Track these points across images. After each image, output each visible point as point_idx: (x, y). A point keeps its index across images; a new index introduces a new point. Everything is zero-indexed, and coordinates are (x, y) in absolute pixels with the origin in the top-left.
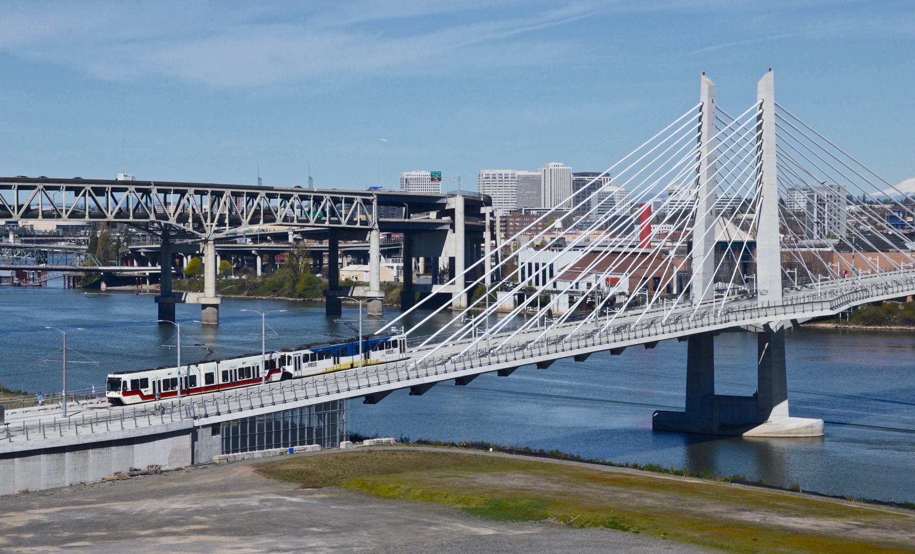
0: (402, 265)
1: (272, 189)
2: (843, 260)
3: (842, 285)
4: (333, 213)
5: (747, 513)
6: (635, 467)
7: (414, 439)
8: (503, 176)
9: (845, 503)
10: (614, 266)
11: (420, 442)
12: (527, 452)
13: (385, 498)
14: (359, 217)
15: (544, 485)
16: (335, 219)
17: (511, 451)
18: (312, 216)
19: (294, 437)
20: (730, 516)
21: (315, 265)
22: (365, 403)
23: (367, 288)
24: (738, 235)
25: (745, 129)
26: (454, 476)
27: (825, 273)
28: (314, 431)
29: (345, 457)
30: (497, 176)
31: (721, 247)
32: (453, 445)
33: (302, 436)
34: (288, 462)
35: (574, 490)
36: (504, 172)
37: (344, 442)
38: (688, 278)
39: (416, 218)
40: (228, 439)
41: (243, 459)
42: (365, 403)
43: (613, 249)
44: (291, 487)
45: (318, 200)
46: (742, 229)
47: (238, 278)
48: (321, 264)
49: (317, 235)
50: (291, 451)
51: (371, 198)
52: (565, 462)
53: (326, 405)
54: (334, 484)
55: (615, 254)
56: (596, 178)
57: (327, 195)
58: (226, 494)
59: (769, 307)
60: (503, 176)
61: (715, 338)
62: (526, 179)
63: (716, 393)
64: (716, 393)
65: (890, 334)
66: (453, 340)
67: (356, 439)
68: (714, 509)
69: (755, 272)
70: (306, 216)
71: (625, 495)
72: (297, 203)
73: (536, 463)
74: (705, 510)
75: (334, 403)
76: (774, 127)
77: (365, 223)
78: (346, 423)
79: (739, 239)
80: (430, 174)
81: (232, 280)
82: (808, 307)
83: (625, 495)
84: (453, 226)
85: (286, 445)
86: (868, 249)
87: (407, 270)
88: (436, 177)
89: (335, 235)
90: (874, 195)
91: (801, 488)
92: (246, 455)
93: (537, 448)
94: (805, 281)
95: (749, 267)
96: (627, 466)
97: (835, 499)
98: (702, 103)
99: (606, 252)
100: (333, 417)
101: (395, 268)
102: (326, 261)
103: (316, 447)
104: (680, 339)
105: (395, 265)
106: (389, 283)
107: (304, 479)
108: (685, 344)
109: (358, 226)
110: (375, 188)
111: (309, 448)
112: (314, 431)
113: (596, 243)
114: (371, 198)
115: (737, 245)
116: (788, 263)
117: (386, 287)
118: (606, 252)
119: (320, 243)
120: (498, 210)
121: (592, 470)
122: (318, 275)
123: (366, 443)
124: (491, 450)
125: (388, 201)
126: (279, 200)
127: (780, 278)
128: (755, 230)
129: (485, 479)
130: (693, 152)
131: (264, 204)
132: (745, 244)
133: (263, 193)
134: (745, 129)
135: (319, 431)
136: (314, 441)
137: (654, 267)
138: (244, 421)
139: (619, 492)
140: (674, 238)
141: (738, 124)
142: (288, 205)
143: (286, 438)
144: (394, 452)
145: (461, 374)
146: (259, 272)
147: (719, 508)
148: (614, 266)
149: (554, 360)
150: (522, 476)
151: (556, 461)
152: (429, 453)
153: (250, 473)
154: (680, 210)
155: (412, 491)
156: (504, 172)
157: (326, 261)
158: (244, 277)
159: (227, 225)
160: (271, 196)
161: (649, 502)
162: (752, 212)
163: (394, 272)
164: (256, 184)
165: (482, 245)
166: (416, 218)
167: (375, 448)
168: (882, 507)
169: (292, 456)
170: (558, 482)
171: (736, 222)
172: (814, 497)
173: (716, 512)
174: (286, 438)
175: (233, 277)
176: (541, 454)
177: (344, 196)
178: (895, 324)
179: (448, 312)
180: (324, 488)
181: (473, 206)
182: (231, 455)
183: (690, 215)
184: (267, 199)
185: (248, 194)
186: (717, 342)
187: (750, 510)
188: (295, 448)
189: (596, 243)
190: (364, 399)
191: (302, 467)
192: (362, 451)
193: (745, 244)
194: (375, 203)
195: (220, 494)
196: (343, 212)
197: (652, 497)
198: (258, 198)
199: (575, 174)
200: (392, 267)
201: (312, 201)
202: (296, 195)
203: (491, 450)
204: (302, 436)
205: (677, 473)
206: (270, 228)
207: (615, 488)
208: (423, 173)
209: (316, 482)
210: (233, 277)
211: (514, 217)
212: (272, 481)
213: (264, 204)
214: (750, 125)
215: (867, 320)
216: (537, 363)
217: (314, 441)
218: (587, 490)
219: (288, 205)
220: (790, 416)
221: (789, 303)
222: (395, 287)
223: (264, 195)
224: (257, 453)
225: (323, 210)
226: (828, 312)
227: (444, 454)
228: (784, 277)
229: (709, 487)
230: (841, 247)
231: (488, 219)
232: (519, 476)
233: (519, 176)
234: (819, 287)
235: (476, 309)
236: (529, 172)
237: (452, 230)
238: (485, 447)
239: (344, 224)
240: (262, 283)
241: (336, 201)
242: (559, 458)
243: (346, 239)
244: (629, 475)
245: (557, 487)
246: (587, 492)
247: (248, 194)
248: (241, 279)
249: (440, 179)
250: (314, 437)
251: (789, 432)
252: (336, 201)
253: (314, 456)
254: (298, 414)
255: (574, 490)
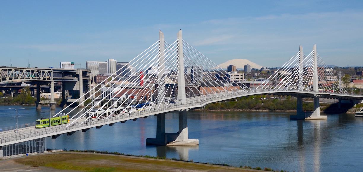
0: (62, 93)
1: (17, 68)
2: (203, 89)
3: (205, 98)
4: (38, 76)
5: (178, 170)
6: (142, 156)
7: (69, 149)
8: (94, 63)
9: (207, 165)
10: (133, 92)
11: (71, 151)
12: (107, 153)
13: (60, 169)
14: (47, 77)
15: (113, 163)
16: (39, 78)
17: (101, 153)
18: (30, 76)
19: (28, 150)
20: (172, 171)
21: (32, 93)
22: (52, 138)
23: (50, 100)
24: (171, 82)
25: (173, 48)
26: (83, 161)
27: (199, 93)
28: (35, 148)
29: (46, 156)
30: (92, 64)
31: (167, 86)
32: (82, 151)
33: (31, 150)
34: (26, 158)
35: (123, 164)
36: (94, 62)
37: (45, 151)
38: (157, 96)
39: (66, 77)
40: (5, 152)
41: (11, 158)
42: (52, 138)
43: (133, 87)
44: (28, 166)
45: (33, 72)
46: (173, 80)
47: (5, 98)
48: (34, 93)
49: (32, 83)
50: (27, 155)
51: (50, 71)
52: (119, 155)
53: (39, 139)
54: (42, 165)
55: (133, 88)
56: (127, 64)
57: (46, 70)
58: (5, 169)
59: (182, 104)
60: (94, 63)
61: (165, 114)
62: (102, 64)
63: (166, 132)
64: (166, 132)
65: (217, 113)
66: (81, 117)
67: (49, 150)
68: (168, 169)
69: (178, 94)
70: (29, 77)
71: (139, 166)
72: (25, 73)
73: (110, 156)
74: (164, 169)
75: (42, 139)
76: (182, 48)
77: (49, 79)
78: (46, 145)
79: (172, 83)
80: (70, 63)
81: (3, 99)
82: (194, 104)
83: (139, 166)
84: (79, 80)
85: (25, 153)
86: (211, 86)
87: (64, 94)
88: (73, 64)
89: (39, 83)
90: (212, 69)
91: (193, 161)
92: (12, 156)
93: (110, 151)
94: (192, 95)
95: (175, 92)
96: (139, 156)
97: (204, 164)
98: (160, 40)
99: (131, 88)
100: (41, 143)
101: (59, 94)
102: (35, 92)
103: (36, 153)
104: (155, 115)
105: (59, 93)
106: (57, 99)
107: (32, 164)
108: (156, 117)
109: (47, 80)
110: (51, 68)
111: (33, 154)
112: (35, 148)
113: (127, 85)
114: (50, 71)
115: (172, 85)
116: (187, 89)
117: (57, 100)
118: (131, 88)
119: (34, 86)
120: (92, 75)
121: (128, 158)
122: (33, 96)
123: (54, 151)
124: (95, 152)
125: (57, 72)
126: (7, 71)
127: (185, 95)
128: (177, 81)
129: (94, 162)
130: (158, 56)
131: (14, 73)
132: (174, 85)
133: (13, 70)
134: (173, 48)
135: (37, 148)
136: (35, 151)
137: (146, 93)
138: (11, 145)
139: (137, 164)
140: (152, 83)
141: (171, 47)
142: (22, 73)
143: (25, 151)
144: (63, 154)
145: (55, 134)
146: (12, 96)
147: (169, 168)
148: (133, 92)
149: (126, 121)
150: (106, 160)
151: (116, 155)
152: (74, 154)
153: (14, 162)
154: (154, 74)
155: (69, 167)
156: (94, 62)
157: (35, 92)
158: (7, 97)
159: (1, 80)
160: (16, 70)
161: (147, 167)
162: (176, 75)
163: (59, 95)
164: (10, 66)
165: (88, 86)
166: (66, 77)
167: (56, 153)
168: (218, 166)
169: (27, 157)
170: (117, 162)
171: (171, 78)
172: (197, 164)
173: (168, 170)
174: (25, 151)
175: (3, 97)
176: (111, 153)
177: (42, 70)
178: (219, 109)
179: (80, 108)
180: (39, 167)
181: (85, 74)
182: (6, 156)
183: (157, 76)
184: (15, 71)
185: (8, 70)
186: (166, 116)
187: (179, 169)
188: (28, 154)
189: (127, 85)
190: (52, 137)
191: (31, 160)
192: (52, 154)
193: (174, 85)
194: (52, 73)
195: (3, 170)
196: (41, 75)
197: (148, 166)
198: (12, 71)
199: (118, 63)
200: (58, 94)
201: (30, 72)
202: (25, 70)
203: (95, 152)
204: (31, 150)
205: (155, 158)
206: (16, 81)
207: (136, 163)
208: (67, 63)
209: (37, 165)
210: (3, 97)
211: (98, 77)
212: (21, 165)
213: (14, 73)
214: (175, 47)
215: (209, 108)
216: (67, 133)
217: (35, 151)
218: (127, 164)
219: (22, 73)
220: (189, 139)
221: (188, 103)
222: (59, 100)
223: (25, 70)
224: (16, 156)
225: (34, 75)
226: (200, 106)
227: (79, 154)
228: (186, 95)
229: (165, 162)
230: (203, 85)
231: (90, 77)
232: (104, 160)
233: (99, 63)
234: (197, 98)
235: (90, 107)
236: (103, 62)
237: (78, 81)
238: (93, 152)
239: (42, 79)
240: (13, 100)
241: (39, 72)
242: (117, 154)
243: (42, 85)
244: (140, 159)
245: (117, 164)
246: (127, 165)
247: (8, 70)
248: (6, 98)
249: (74, 65)
250: (35, 150)
251: (188, 144)
252: (39, 72)
253: (35, 156)
254: (30, 143)
255: (123, 164)
